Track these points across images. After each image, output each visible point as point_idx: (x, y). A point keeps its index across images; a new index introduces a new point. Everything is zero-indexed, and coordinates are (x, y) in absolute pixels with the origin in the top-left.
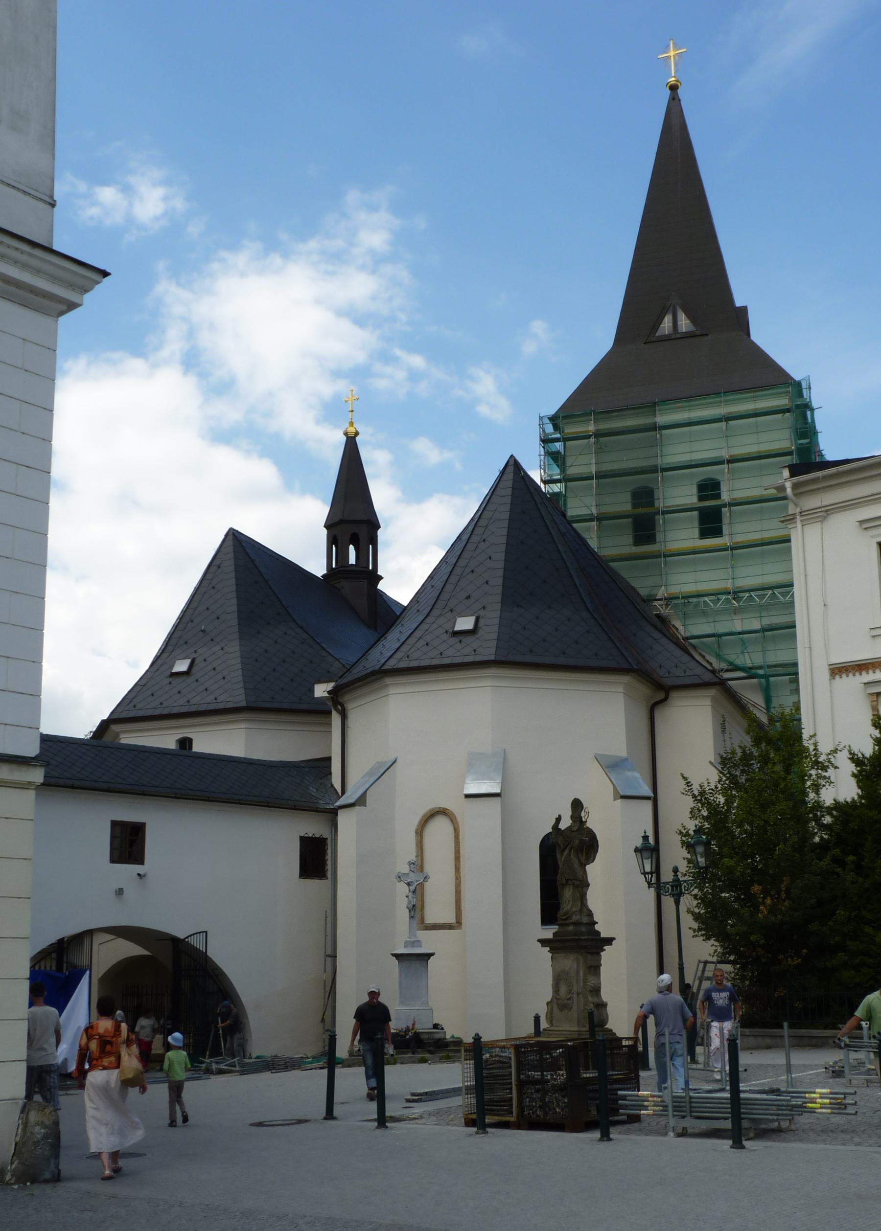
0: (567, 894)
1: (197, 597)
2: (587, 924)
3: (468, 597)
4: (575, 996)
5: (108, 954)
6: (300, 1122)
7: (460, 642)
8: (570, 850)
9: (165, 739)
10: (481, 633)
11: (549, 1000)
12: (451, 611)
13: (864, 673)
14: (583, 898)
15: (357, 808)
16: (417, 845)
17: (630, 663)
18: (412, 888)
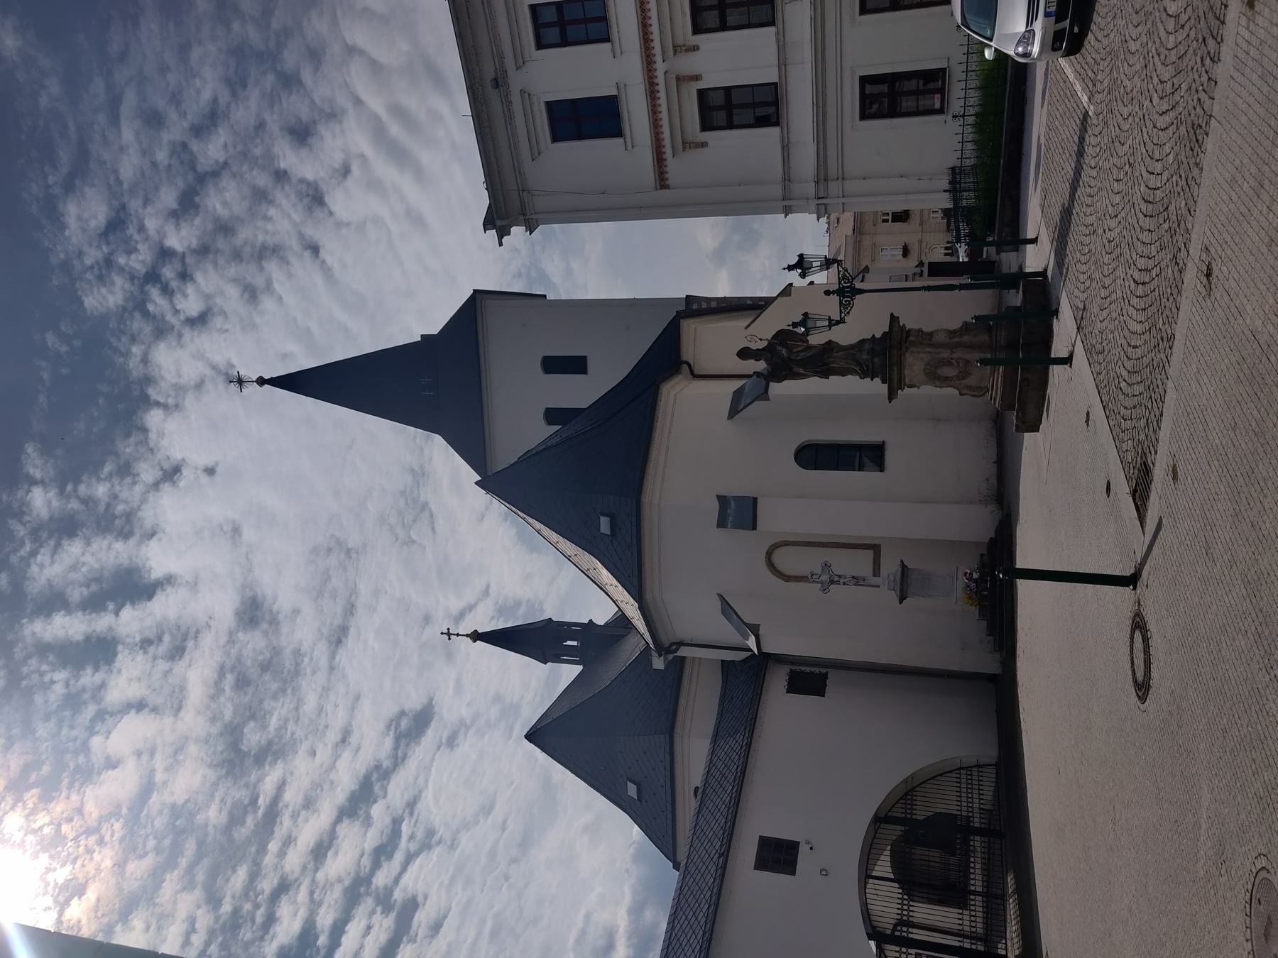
5: (887, 901)
9: (687, 807)
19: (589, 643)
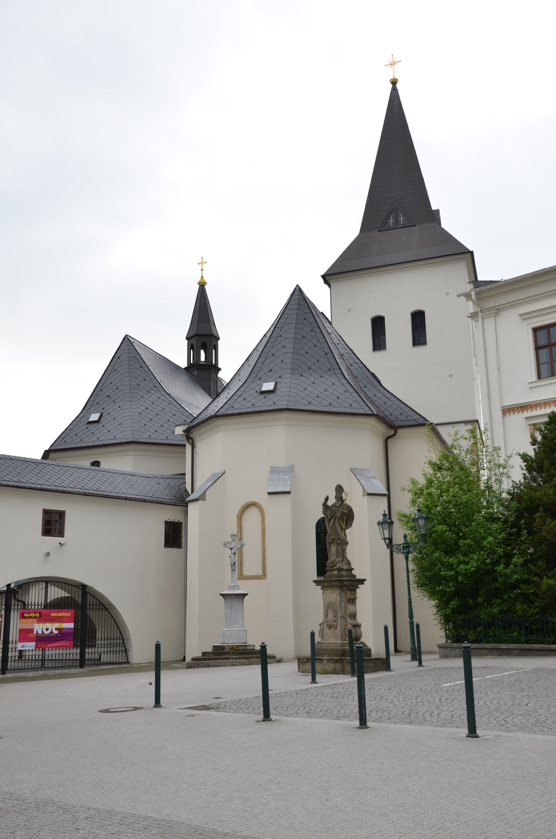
0: (333, 550)
1: (105, 377)
2: (347, 570)
3: (271, 371)
4: (339, 619)
6: (136, 709)
7: (265, 397)
8: (335, 520)
10: (278, 392)
11: (321, 622)
12: (260, 379)
13: (525, 412)
14: (344, 551)
15: (200, 502)
16: (238, 525)
17: (372, 410)
18: (233, 551)
19: (202, 372)
